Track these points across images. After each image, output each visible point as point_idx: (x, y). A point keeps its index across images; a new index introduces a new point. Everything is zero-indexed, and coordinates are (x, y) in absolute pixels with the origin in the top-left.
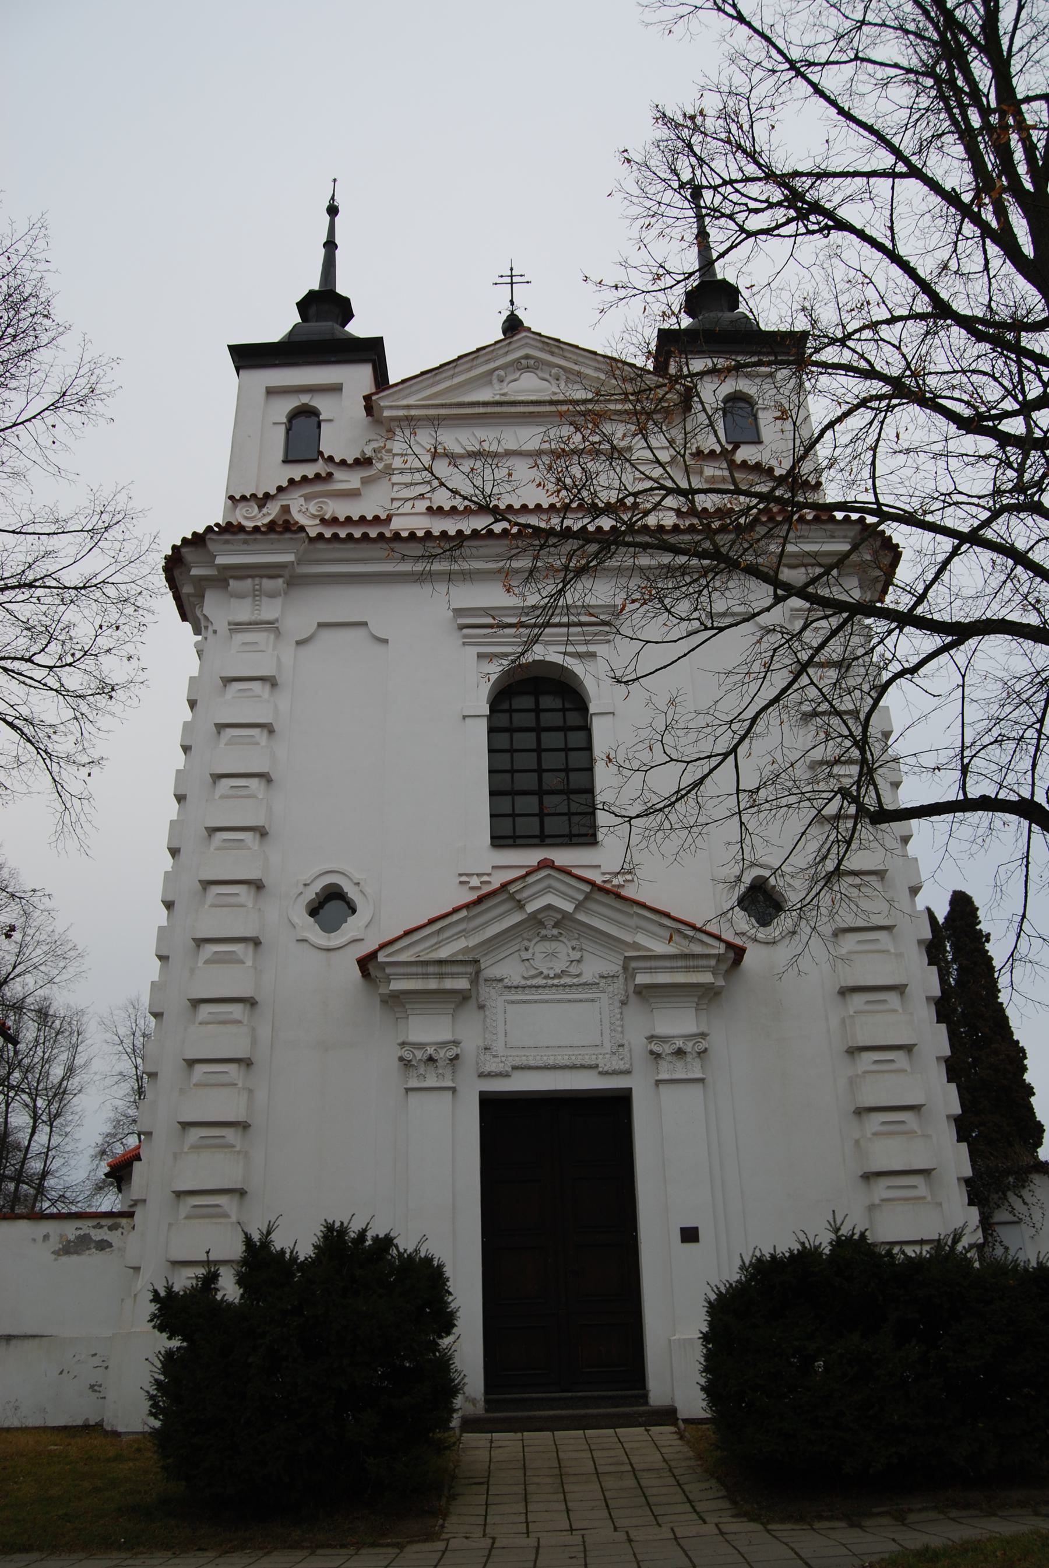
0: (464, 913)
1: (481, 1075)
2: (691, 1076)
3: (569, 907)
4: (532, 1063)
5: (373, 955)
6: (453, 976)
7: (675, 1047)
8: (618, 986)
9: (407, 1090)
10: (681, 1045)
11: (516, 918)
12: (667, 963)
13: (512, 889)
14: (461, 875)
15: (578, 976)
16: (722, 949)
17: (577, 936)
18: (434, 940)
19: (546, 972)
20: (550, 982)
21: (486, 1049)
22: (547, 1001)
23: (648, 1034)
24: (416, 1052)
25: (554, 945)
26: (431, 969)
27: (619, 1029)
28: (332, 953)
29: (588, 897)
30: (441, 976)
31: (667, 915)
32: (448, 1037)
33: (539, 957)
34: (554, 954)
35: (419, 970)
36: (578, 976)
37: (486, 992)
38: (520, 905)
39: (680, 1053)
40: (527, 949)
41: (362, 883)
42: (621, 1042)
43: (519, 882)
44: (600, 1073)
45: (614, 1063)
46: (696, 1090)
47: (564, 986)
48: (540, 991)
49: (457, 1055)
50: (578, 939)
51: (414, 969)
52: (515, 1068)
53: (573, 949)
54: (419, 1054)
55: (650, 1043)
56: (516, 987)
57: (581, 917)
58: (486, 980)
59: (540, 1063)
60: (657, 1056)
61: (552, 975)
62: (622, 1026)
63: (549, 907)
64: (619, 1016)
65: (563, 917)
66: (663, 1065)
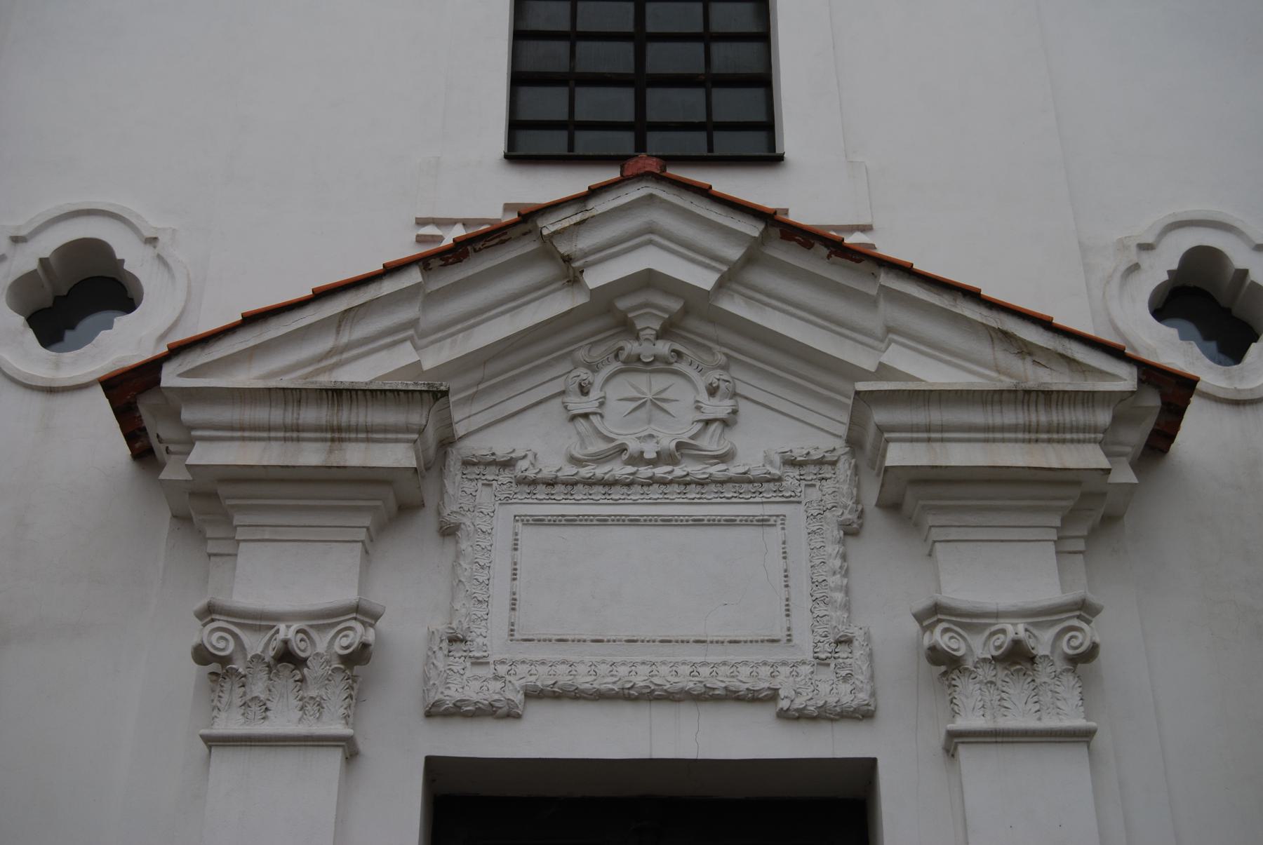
0: (414, 277)
1: (434, 712)
2: (1050, 722)
3: (705, 279)
4: (584, 681)
5: (147, 373)
6: (369, 434)
7: (1004, 641)
8: (838, 486)
9: (212, 742)
10: (1022, 634)
11: (560, 303)
12: (976, 416)
13: (549, 225)
14: (421, 222)
15: (724, 458)
16: (1125, 379)
17: (721, 359)
18: (326, 343)
19: (634, 446)
20: (645, 472)
21: (453, 640)
22: (634, 522)
23: (923, 603)
24: (247, 638)
25: (659, 382)
26: (311, 415)
27: (839, 596)
28: (60, 401)
29: (752, 258)
30: (337, 434)
31: (972, 295)
32: (347, 595)
33: (616, 409)
34: (658, 403)
35: (276, 415)
36: (724, 458)
37: (460, 493)
38: (573, 279)
39: (1017, 657)
40: (584, 390)
41: (164, 239)
42: (843, 630)
43: (569, 211)
44: (784, 715)
45: (824, 688)
46: (1067, 765)
47: (685, 482)
48: (617, 493)
49: (365, 646)
50: (724, 368)
51: (260, 414)
52: (534, 695)
53: (712, 391)
54: (255, 644)
55: (930, 628)
56: (551, 483)
57: (735, 306)
58: (467, 463)
59: (606, 683)
60: (946, 663)
61: (650, 455)
62: (847, 590)
63: (649, 280)
64: (838, 562)
65: (686, 311)
66: (969, 692)
